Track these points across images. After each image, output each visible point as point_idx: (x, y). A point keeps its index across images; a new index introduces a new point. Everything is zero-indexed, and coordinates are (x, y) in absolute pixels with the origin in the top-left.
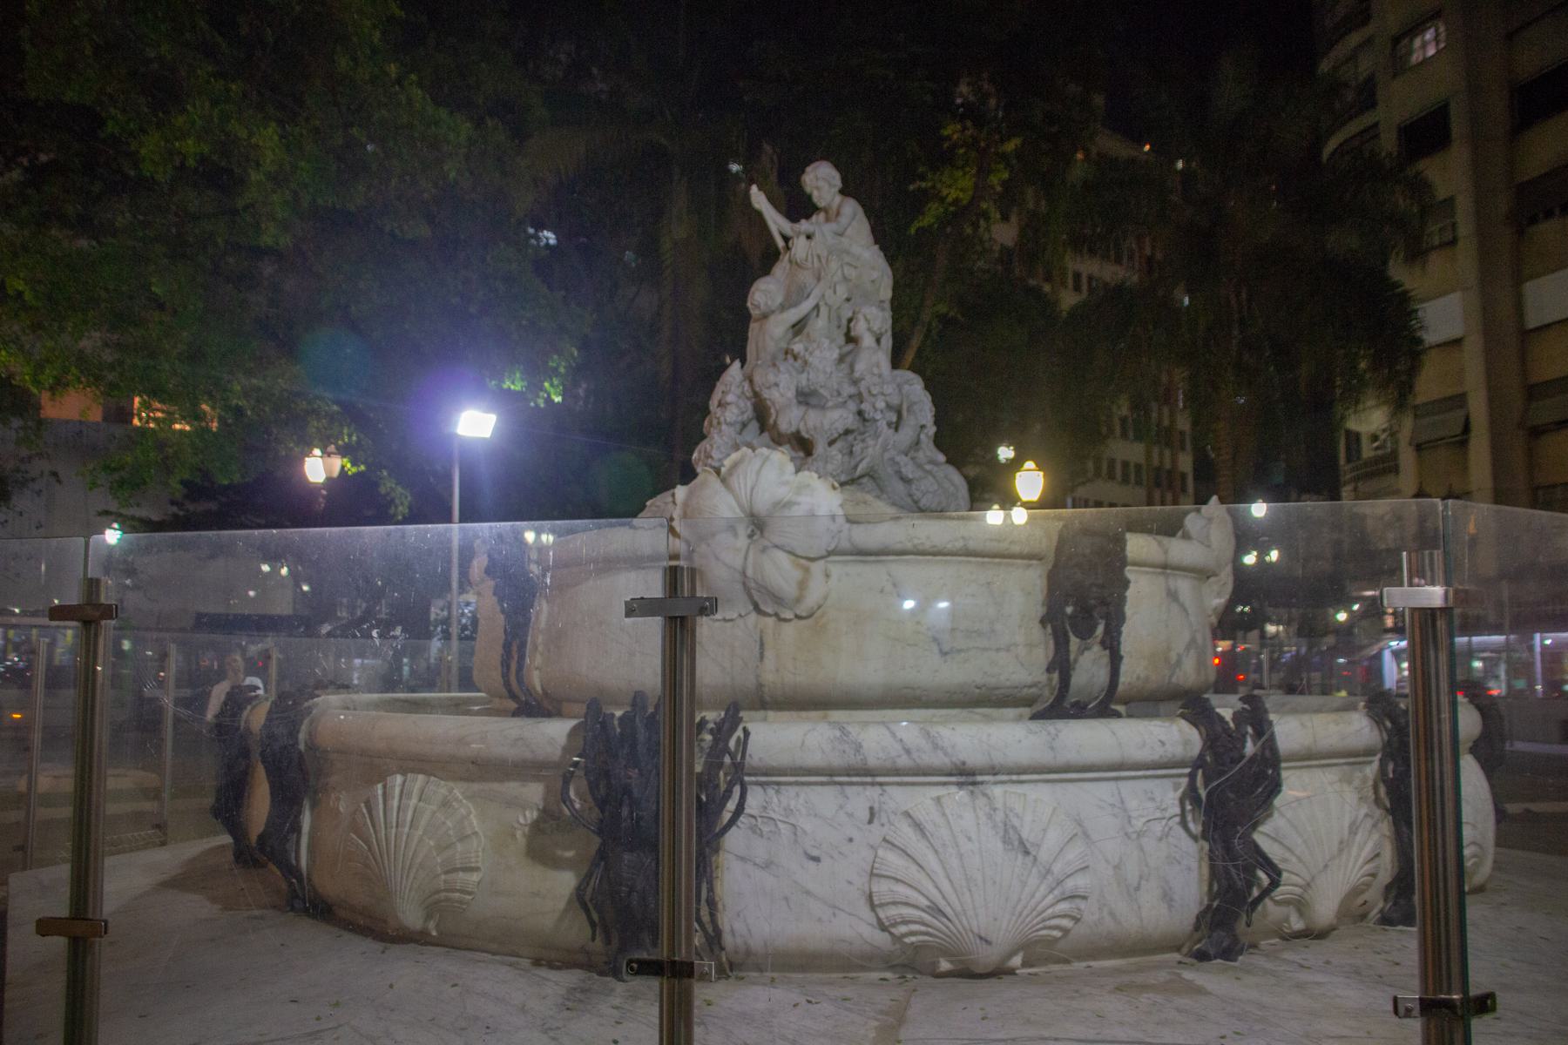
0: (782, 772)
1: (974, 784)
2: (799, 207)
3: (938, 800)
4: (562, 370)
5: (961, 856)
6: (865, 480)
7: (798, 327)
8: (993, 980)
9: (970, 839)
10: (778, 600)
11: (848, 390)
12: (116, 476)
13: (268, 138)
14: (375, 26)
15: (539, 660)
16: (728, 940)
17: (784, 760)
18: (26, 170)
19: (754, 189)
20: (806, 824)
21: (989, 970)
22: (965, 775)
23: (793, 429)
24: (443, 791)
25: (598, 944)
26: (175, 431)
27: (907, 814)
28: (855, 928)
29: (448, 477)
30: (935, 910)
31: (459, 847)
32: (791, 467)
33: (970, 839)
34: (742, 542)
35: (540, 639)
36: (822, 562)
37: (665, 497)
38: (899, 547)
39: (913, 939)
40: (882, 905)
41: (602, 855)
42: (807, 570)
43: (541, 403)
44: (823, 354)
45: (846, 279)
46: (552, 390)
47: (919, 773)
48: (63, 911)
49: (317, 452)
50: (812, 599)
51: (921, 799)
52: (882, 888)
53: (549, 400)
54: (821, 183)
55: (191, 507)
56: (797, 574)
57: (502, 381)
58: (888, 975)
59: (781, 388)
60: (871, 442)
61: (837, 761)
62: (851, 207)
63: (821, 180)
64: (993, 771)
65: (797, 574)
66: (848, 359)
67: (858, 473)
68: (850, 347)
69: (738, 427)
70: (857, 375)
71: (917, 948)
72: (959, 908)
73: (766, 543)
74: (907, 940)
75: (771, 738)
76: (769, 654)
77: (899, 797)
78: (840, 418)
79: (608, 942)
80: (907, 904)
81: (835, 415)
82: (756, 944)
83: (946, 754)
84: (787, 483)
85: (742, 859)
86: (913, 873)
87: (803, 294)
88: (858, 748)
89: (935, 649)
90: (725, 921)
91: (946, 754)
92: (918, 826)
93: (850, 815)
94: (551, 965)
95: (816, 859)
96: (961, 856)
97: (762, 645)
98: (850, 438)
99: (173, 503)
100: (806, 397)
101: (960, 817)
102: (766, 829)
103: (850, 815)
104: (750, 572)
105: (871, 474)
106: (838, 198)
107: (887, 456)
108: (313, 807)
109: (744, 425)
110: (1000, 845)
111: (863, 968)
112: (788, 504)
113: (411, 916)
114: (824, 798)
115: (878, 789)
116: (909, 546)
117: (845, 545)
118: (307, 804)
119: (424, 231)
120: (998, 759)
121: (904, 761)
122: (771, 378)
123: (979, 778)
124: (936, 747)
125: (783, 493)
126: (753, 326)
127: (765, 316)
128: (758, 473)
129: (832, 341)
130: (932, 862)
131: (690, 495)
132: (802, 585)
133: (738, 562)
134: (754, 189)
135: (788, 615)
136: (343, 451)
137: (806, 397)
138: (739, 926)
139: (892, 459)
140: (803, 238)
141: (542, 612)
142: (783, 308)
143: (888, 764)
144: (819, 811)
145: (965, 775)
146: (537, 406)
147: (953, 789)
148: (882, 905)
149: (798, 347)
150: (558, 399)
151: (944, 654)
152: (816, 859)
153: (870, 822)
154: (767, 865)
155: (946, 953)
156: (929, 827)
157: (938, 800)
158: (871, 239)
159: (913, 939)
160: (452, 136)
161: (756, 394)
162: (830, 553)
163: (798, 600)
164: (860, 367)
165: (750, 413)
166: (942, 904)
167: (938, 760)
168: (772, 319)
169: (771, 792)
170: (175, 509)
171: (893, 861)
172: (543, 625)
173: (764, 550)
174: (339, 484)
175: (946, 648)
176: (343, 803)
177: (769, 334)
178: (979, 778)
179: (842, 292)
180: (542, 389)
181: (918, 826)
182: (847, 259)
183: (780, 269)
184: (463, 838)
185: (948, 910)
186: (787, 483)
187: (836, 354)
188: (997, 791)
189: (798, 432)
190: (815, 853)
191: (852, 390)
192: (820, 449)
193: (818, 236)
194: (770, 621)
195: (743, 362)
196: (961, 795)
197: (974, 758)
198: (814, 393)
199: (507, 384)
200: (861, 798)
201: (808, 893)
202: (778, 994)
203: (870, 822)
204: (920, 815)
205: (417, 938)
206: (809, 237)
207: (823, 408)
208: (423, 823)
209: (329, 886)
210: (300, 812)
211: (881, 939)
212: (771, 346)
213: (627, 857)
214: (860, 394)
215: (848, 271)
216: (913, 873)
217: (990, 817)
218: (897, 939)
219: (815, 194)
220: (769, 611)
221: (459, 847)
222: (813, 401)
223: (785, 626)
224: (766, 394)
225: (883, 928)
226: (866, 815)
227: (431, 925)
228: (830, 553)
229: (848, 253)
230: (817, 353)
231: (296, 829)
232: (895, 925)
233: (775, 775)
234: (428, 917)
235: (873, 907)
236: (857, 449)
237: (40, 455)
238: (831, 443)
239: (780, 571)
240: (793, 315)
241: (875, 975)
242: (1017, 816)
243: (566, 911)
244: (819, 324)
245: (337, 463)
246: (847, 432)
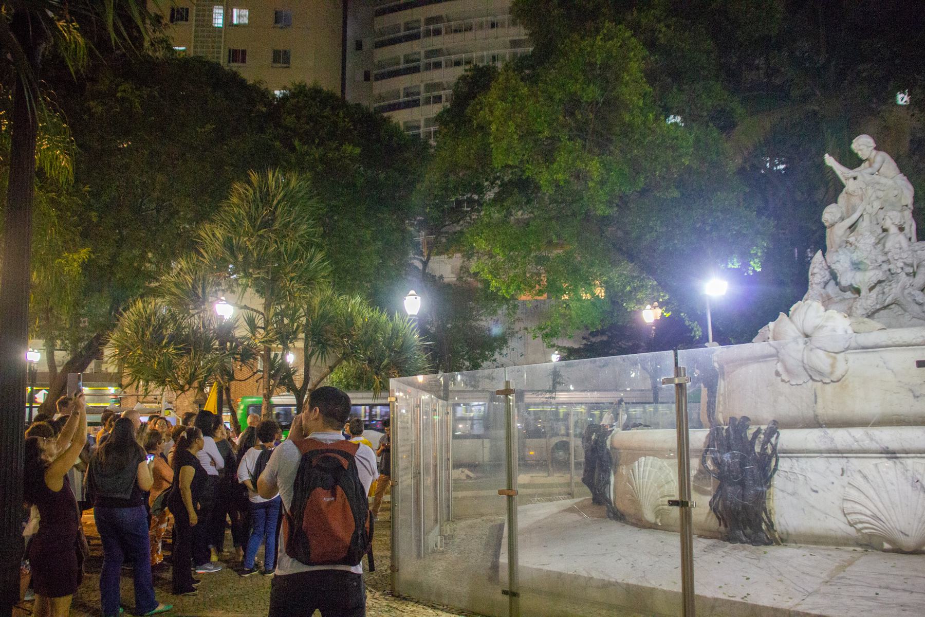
0: (799, 452)
1: (897, 458)
2: (853, 161)
3: (876, 465)
4: (759, 254)
5: (887, 492)
6: (893, 306)
7: (853, 227)
8: (914, 556)
9: (892, 484)
10: (821, 373)
11: (881, 258)
12: (544, 332)
13: (594, 167)
14: (639, 99)
15: (721, 409)
16: (777, 527)
17: (798, 446)
18: (500, 186)
19: (827, 156)
20: (810, 475)
21: (910, 550)
22: (890, 454)
23: (849, 284)
24: (660, 463)
25: (722, 528)
26: (17, 568)
27: (860, 471)
28: (837, 525)
29: (705, 315)
30: (875, 517)
31: (666, 486)
32: (822, 308)
33: (892, 484)
34: (801, 346)
35: (721, 399)
36: (842, 354)
37: (765, 328)
38: (884, 343)
39: (867, 531)
40: (849, 514)
41: (720, 488)
42: (835, 358)
43: (751, 273)
44: (865, 240)
45: (878, 198)
46: (755, 266)
47: (863, 452)
48: (505, 488)
49: (649, 307)
50: (838, 373)
51: (868, 465)
52: (848, 506)
53: (754, 271)
54: (862, 147)
55: (593, 340)
56: (830, 361)
57: (727, 264)
58: (859, 549)
59: (841, 261)
60: (894, 285)
61: (823, 447)
62: (882, 156)
63: (863, 145)
64: (906, 452)
65: (830, 361)
66: (882, 241)
67: (886, 303)
68: (884, 234)
69: (822, 285)
70: (886, 250)
71: (871, 536)
72: (888, 517)
73: (812, 346)
74: (864, 531)
75: (787, 438)
76: (819, 400)
77: (856, 463)
78: (872, 276)
79: (726, 526)
80: (861, 514)
81: (870, 274)
82: (791, 530)
83: (877, 443)
84: (820, 317)
85: (782, 491)
86: (862, 498)
87: (854, 209)
88: (832, 440)
89: (911, 394)
90: (775, 519)
91: (877, 443)
92: (865, 477)
93: (832, 472)
94: (706, 537)
95: (817, 492)
96: (887, 492)
97: (816, 396)
98: (883, 284)
99: (584, 338)
100: (857, 266)
101: (887, 473)
102: (792, 478)
103: (832, 472)
104: (805, 361)
105: (895, 302)
106: (874, 152)
107: (906, 291)
108: (615, 474)
109: (826, 284)
110: (910, 488)
111: (845, 545)
112: (822, 327)
113: (649, 516)
114: (820, 463)
115: (845, 460)
116: (890, 343)
117: (854, 344)
118: (612, 472)
119: (676, 194)
120: (907, 446)
121: (855, 446)
122: (835, 258)
123: (898, 455)
124: (872, 440)
125: (818, 322)
126: (828, 230)
127: (832, 225)
128: (806, 313)
129: (872, 232)
130: (872, 493)
131: (775, 326)
132: (833, 366)
133: (799, 356)
134: (827, 156)
135: (827, 381)
136: (661, 305)
137: (857, 266)
138: (782, 521)
139: (909, 293)
140: (852, 180)
141: (722, 386)
142: (842, 219)
143: (848, 448)
144: (818, 470)
145: (890, 454)
146: (749, 275)
147: (885, 460)
148: (849, 514)
149: (852, 239)
150: (759, 270)
151: (916, 397)
152: (817, 492)
153: (842, 475)
154: (794, 494)
155: (889, 541)
156: (870, 477)
157: (876, 465)
158: (897, 170)
159: (867, 531)
160: (684, 144)
161: (829, 267)
162: (847, 349)
163: (832, 373)
164: (889, 245)
165: (828, 276)
166: (879, 514)
167: (874, 446)
168: (836, 226)
169: (794, 460)
170: (585, 342)
171: (854, 494)
172: (722, 391)
173: (811, 350)
174: (663, 324)
175: (917, 394)
176: (623, 470)
177: (836, 234)
178: (898, 455)
179: (877, 205)
180: (750, 265)
181: (865, 477)
182: (878, 187)
183: (842, 198)
184: (668, 483)
185: (882, 518)
186: (820, 317)
187: (873, 240)
188: (909, 462)
189: (851, 285)
190: (815, 489)
191: (884, 258)
192: (864, 292)
193: (859, 178)
194: (820, 384)
195: (824, 251)
196: (890, 463)
197: (893, 446)
198: (861, 263)
199: (730, 266)
200: (837, 464)
201: (813, 507)
202: (800, 551)
203: (842, 475)
204: (866, 472)
205: (652, 527)
206: (855, 178)
207: (865, 270)
208: (652, 477)
209: (620, 506)
210: (609, 476)
211: (851, 531)
212: (837, 241)
213: (730, 488)
214: (888, 260)
215: (880, 194)
216: (862, 498)
217: (904, 474)
218: (859, 530)
219: (860, 153)
220: (817, 379)
221: (666, 486)
222: (862, 267)
223: (827, 386)
224: (833, 267)
225: (851, 525)
226: (840, 472)
227: (658, 520)
228: (847, 349)
229: (878, 183)
230: (862, 241)
231: (608, 483)
232: (856, 523)
233: (790, 453)
234: (657, 517)
235: (845, 515)
236: (886, 290)
237: (518, 320)
238: (871, 289)
239: (821, 360)
240: (848, 222)
241: (851, 548)
242: (920, 474)
243: (709, 513)
244: (864, 225)
245: (659, 311)
246: (880, 282)
